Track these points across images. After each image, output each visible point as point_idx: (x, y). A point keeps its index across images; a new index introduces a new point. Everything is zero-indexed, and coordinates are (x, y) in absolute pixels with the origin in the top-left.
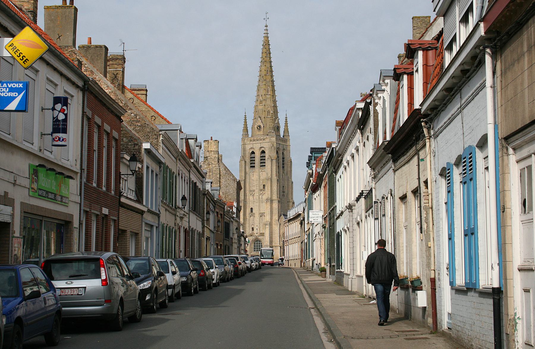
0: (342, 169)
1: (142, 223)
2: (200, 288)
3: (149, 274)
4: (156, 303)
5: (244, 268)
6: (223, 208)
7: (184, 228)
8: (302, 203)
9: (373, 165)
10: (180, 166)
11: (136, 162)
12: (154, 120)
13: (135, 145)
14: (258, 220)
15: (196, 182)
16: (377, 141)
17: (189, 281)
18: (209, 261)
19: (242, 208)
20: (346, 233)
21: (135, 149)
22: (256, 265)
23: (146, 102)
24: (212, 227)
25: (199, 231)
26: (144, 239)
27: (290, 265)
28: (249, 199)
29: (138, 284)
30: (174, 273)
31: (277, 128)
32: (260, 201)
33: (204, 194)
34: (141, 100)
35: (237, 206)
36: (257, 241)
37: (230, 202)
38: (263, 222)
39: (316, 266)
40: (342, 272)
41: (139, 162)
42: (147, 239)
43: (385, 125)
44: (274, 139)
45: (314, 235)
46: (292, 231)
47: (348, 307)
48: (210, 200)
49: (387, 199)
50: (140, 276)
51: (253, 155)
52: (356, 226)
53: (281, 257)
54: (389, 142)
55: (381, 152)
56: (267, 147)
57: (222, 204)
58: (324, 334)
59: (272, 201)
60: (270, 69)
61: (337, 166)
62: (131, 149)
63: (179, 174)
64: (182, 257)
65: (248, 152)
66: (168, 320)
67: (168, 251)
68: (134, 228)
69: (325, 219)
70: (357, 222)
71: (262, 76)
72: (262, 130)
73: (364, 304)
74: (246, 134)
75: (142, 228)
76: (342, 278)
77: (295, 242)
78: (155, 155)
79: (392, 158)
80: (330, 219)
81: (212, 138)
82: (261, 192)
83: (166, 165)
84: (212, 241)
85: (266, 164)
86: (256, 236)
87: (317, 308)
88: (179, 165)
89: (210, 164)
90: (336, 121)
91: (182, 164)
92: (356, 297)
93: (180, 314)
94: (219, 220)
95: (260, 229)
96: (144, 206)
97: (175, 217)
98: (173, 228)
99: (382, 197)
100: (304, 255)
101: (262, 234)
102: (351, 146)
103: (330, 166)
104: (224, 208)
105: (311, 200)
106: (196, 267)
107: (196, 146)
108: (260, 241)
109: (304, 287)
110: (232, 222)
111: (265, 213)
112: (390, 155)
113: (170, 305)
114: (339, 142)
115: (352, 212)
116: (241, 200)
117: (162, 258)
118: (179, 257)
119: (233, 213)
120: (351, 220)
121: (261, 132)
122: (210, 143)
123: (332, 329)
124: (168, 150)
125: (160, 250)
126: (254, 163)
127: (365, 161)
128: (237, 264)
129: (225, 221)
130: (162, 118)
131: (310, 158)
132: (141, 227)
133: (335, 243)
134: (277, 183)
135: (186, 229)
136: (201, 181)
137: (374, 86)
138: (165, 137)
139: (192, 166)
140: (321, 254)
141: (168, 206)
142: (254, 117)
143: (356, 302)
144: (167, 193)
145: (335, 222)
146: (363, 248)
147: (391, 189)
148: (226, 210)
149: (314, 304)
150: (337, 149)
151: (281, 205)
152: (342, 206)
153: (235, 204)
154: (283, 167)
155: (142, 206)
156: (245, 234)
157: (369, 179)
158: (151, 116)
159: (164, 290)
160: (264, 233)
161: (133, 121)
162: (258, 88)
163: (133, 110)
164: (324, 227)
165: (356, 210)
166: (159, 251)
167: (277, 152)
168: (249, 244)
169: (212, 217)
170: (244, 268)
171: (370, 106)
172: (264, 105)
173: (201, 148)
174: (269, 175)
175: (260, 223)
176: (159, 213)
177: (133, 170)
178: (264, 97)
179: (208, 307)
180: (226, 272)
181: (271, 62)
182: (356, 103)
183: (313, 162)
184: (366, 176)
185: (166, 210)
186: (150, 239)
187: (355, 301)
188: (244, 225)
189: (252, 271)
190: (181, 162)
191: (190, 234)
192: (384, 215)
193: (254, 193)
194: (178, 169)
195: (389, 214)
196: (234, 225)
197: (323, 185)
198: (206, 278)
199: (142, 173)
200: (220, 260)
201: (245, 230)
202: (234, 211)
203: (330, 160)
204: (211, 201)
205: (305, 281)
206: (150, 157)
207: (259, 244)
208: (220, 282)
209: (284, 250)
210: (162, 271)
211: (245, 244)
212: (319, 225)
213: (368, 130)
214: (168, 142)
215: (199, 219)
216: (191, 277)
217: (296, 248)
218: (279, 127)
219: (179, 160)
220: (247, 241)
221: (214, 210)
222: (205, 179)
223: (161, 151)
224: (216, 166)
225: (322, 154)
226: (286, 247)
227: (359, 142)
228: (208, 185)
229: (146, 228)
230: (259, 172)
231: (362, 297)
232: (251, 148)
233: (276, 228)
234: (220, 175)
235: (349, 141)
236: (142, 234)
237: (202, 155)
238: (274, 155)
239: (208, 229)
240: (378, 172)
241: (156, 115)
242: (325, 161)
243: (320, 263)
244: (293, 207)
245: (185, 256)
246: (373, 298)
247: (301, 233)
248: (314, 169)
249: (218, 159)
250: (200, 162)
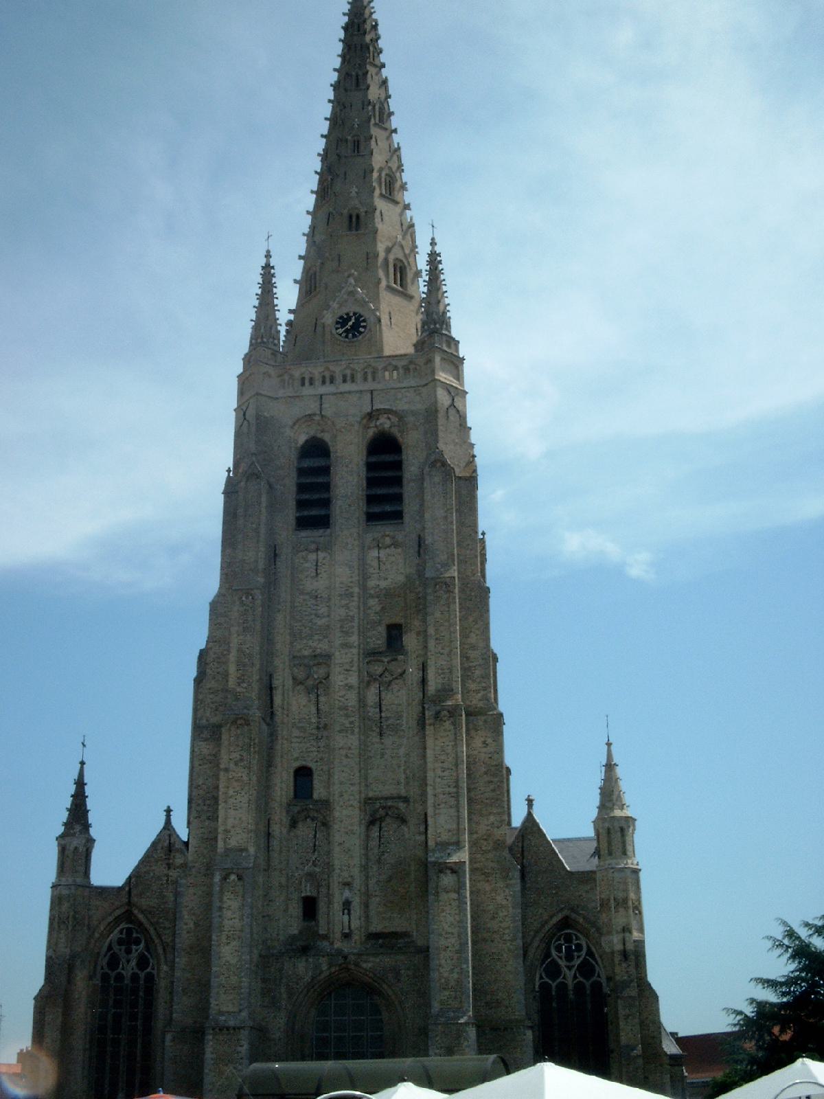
56: (414, 413)
82: (377, 669)
95: (366, 905)
175: (365, 868)
230: (363, 549)
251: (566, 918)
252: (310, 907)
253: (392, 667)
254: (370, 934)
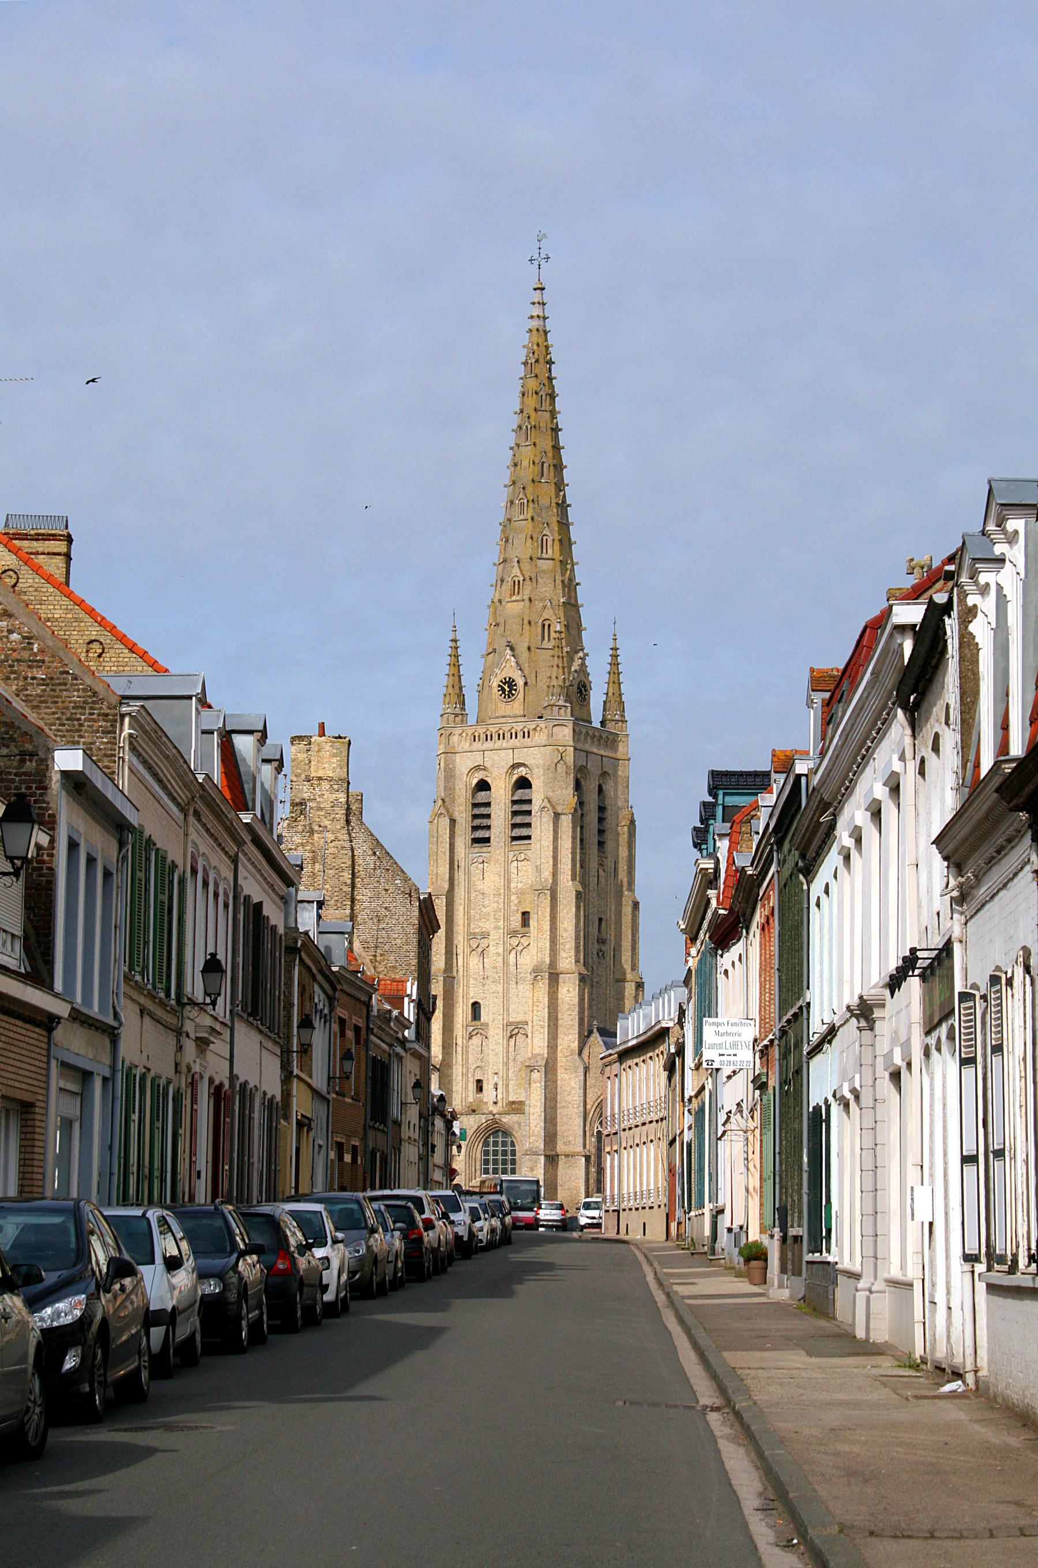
0: (832, 859)
1: (48, 1063)
2: (271, 1322)
3: (79, 1267)
4: (104, 1384)
5: (443, 1243)
6: (364, 1003)
7: (211, 1081)
8: (673, 985)
9: (957, 849)
10: (199, 841)
11: (30, 825)
12: (100, 656)
13: (25, 755)
14: (500, 1049)
15: (261, 903)
16: (972, 757)
17: (232, 1296)
18: (309, 1216)
19: (439, 1003)
20: (848, 1113)
21: (25, 774)
22: (493, 1230)
23: (67, 583)
24: (319, 1080)
25: (269, 1096)
26: (53, 1120)
27: (623, 1230)
28: (466, 966)
29: (37, 1306)
30: (173, 1264)
31: (579, 692)
32: (509, 976)
33: (292, 950)
34: (49, 579)
35: (418, 994)
36: (495, 1133)
37: (393, 980)
38: (519, 1058)
39: (729, 1239)
40: (829, 1263)
41: (40, 824)
42: (67, 1125)
43: (1003, 694)
44: (565, 733)
45: (722, 1117)
46: (634, 1098)
47: (856, 1405)
48: (314, 970)
49: (1011, 986)
50: (42, 1280)
51: (482, 796)
52: (885, 1085)
53: (587, 1196)
54: (1021, 762)
55: (988, 803)
57: (361, 989)
58: (759, 1515)
59: (554, 978)
60: (554, 458)
61: (814, 846)
62: (10, 773)
63: (194, 871)
64: (203, 1201)
65: (468, 781)
66: (150, 1451)
67: (147, 1171)
68: (17, 1084)
69: (764, 1052)
70: (891, 1070)
71: (520, 485)
72: (521, 696)
73: (917, 1397)
74: (458, 711)
75: (47, 1082)
76: (831, 1288)
77: (644, 1139)
78: (114, 806)
79: (1030, 826)
80: (784, 1055)
81: (322, 726)
82: (515, 941)
83: (147, 834)
84: (319, 1135)
85: (535, 832)
86: (491, 1113)
87: (734, 1409)
88: (196, 834)
89: (316, 828)
90: (812, 670)
91: (208, 831)
92: (886, 1365)
93: (197, 1427)
94: (349, 1050)
95: (507, 1086)
96: (56, 995)
97: (179, 1041)
98: (169, 1082)
99: (991, 976)
100: (678, 1191)
101: (517, 1107)
102: (869, 770)
103: (786, 846)
104: (368, 1005)
105: (711, 974)
106: (259, 1241)
107: (264, 761)
108: (506, 1134)
109: (681, 1321)
110: (400, 1058)
111: (527, 1023)
112: (1023, 816)
113: (156, 1388)
114: (823, 754)
115: (872, 1029)
116: (433, 969)
117: (124, 1201)
118: (192, 1198)
119: (404, 1024)
120: (867, 1059)
121: (517, 706)
122: (314, 748)
123: (791, 1495)
124: (155, 775)
125: (116, 1170)
126: (488, 827)
127: (923, 831)
128: (418, 1227)
129: (372, 1053)
130: (131, 651)
131: (707, 811)
132: (44, 1079)
133: (802, 1150)
134: (578, 908)
135: (221, 1085)
136: (282, 898)
137: (964, 543)
138: (141, 727)
139: (247, 838)
140: (747, 1190)
141: (151, 996)
142: (490, 644)
143: (885, 1385)
144: (146, 943)
145: (805, 1065)
146: (912, 1175)
147: (1024, 948)
148: (375, 1012)
149: (722, 1390)
150: (816, 780)
151: (591, 994)
152: (831, 1004)
153: (412, 988)
154: (601, 844)
155: (50, 997)
156: (451, 1104)
157: (941, 904)
158: (87, 639)
159: (133, 1332)
160: (521, 1103)
161: (18, 661)
162: (503, 531)
163: (17, 619)
164: (760, 1084)
165: (886, 1023)
166: (111, 1174)
167: (578, 786)
168: (463, 1144)
169: (319, 1039)
170: (443, 1243)
171: (946, 618)
172: (526, 597)
173: (279, 768)
174: (547, 874)
175: (506, 1064)
176: (115, 1024)
177: (18, 858)
178: (526, 566)
179: (305, 1400)
180: (374, 1259)
181: (556, 430)
182: (891, 607)
183: (719, 826)
184: (929, 891)
185: (143, 1011)
186: (76, 1126)
187: (884, 1381)
188: (445, 1069)
189: (476, 1253)
190: (204, 825)
191: (234, 1104)
192: (998, 1049)
193: (484, 944)
194: (190, 850)
195: (1016, 1043)
196: (406, 1072)
197: (758, 918)
198: (295, 1285)
199: (51, 869)
200: (352, 1209)
201: (450, 1091)
202: (406, 1015)
203: (787, 821)
204: (319, 977)
205: (683, 1298)
206: (80, 804)
207: (504, 1144)
208: (352, 1298)
209: (601, 1170)
210: (126, 1256)
211: (447, 1145)
212: (740, 1078)
213: (938, 711)
214: (155, 743)
215: (269, 1045)
216: (241, 1278)
217: (648, 1162)
218: (584, 686)
219: (197, 814)
220: (457, 1132)
221: (331, 1010)
222: (297, 890)
223: (124, 781)
224: (341, 837)
225: (752, 798)
226: (608, 1157)
227: (902, 758)
228: (306, 914)
229: (62, 1084)
230: (508, 863)
231: (910, 1367)
232: (478, 768)
233: (569, 1082)
234: (353, 874)
235: (863, 751)
236: (46, 1108)
237: (283, 794)
238: (567, 797)
239: (305, 1087)
240: (976, 876)
241: (106, 638)
242: (768, 825)
243: (741, 1227)
244: (636, 1001)
245: (215, 1196)
246: (953, 1373)
247: (669, 1102)
248: (722, 855)
249: (348, 809)
250: (277, 819)
252: (479, 1086)
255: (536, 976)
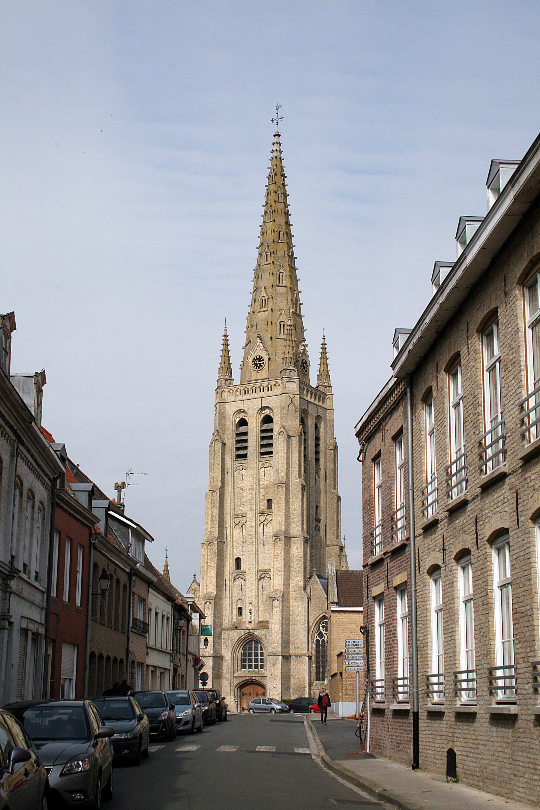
28: (232, 535)
82: (263, 519)
86: (247, 629)
95: (258, 611)
175: (257, 597)
232: (240, 411)
251: (324, 616)
253: (267, 517)
254: (259, 621)
255: (276, 539)
